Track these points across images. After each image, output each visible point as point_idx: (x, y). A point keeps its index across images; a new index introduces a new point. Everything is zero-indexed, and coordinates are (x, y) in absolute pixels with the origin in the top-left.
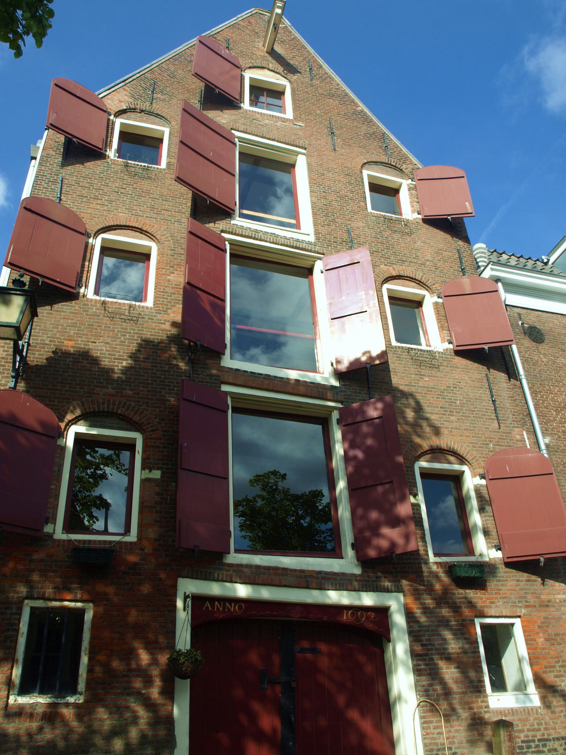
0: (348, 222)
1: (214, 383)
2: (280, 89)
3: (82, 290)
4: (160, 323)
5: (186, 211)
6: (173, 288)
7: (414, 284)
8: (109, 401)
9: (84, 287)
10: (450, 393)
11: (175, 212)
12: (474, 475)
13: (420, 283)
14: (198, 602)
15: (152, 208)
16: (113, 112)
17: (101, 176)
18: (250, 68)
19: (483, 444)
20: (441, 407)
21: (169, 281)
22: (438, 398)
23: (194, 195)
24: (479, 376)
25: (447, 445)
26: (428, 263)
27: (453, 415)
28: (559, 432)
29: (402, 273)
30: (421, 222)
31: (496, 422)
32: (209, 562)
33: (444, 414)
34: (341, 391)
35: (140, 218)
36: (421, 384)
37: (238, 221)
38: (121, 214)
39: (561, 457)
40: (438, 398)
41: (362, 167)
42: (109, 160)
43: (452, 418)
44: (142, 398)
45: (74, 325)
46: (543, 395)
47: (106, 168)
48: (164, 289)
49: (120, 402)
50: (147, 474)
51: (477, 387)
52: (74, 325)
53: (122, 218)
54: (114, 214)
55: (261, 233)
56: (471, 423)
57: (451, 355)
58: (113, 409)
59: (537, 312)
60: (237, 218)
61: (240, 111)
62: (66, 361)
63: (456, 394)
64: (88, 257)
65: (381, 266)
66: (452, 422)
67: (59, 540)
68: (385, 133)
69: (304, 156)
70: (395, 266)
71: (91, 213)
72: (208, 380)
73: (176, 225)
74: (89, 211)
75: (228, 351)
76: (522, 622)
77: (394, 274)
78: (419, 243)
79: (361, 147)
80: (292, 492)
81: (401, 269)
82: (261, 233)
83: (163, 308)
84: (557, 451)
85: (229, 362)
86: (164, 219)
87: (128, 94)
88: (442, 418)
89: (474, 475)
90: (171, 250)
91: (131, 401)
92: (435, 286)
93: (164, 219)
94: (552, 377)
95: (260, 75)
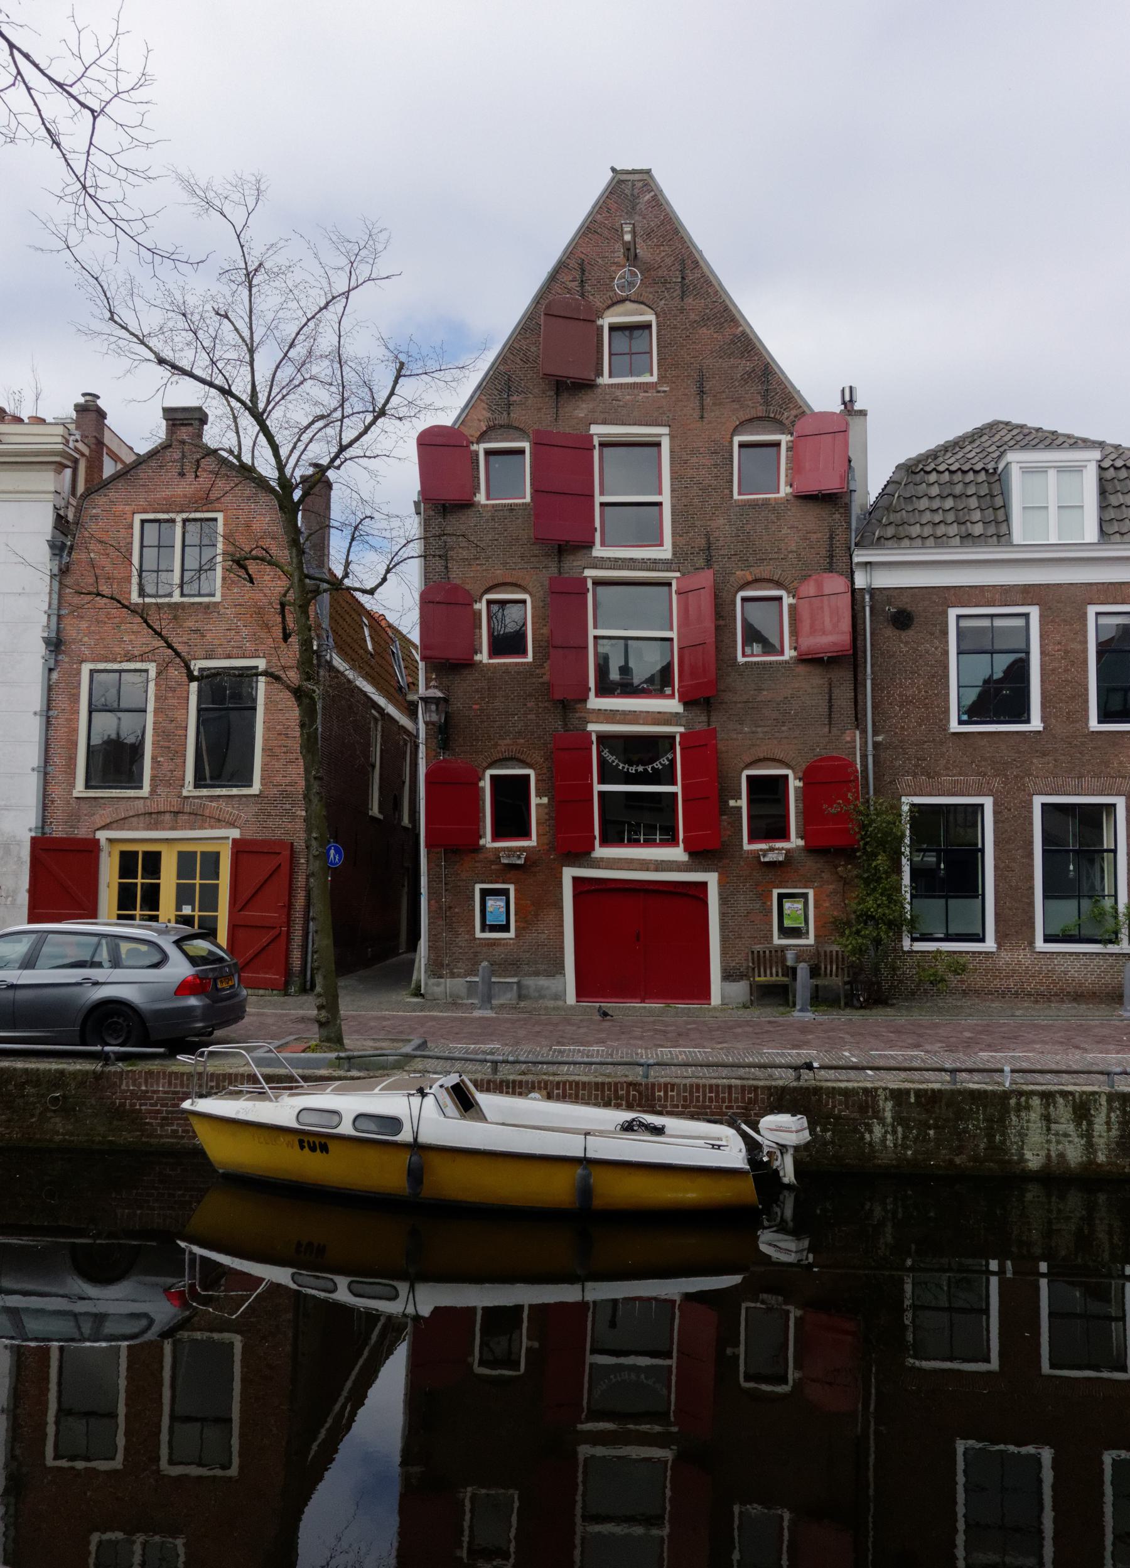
13: (779, 584)
14: (576, 880)
18: (608, 307)
23: (216, 938)
24: (821, 682)
29: (758, 576)
32: (580, 854)
36: (759, 699)
41: (734, 430)
45: (477, 691)
50: (539, 801)
52: (477, 691)
53: (500, 574)
62: (659, 1091)
70: (752, 569)
77: (750, 579)
80: (99, 402)
85: (595, 703)
89: (795, 778)
95: (620, 315)
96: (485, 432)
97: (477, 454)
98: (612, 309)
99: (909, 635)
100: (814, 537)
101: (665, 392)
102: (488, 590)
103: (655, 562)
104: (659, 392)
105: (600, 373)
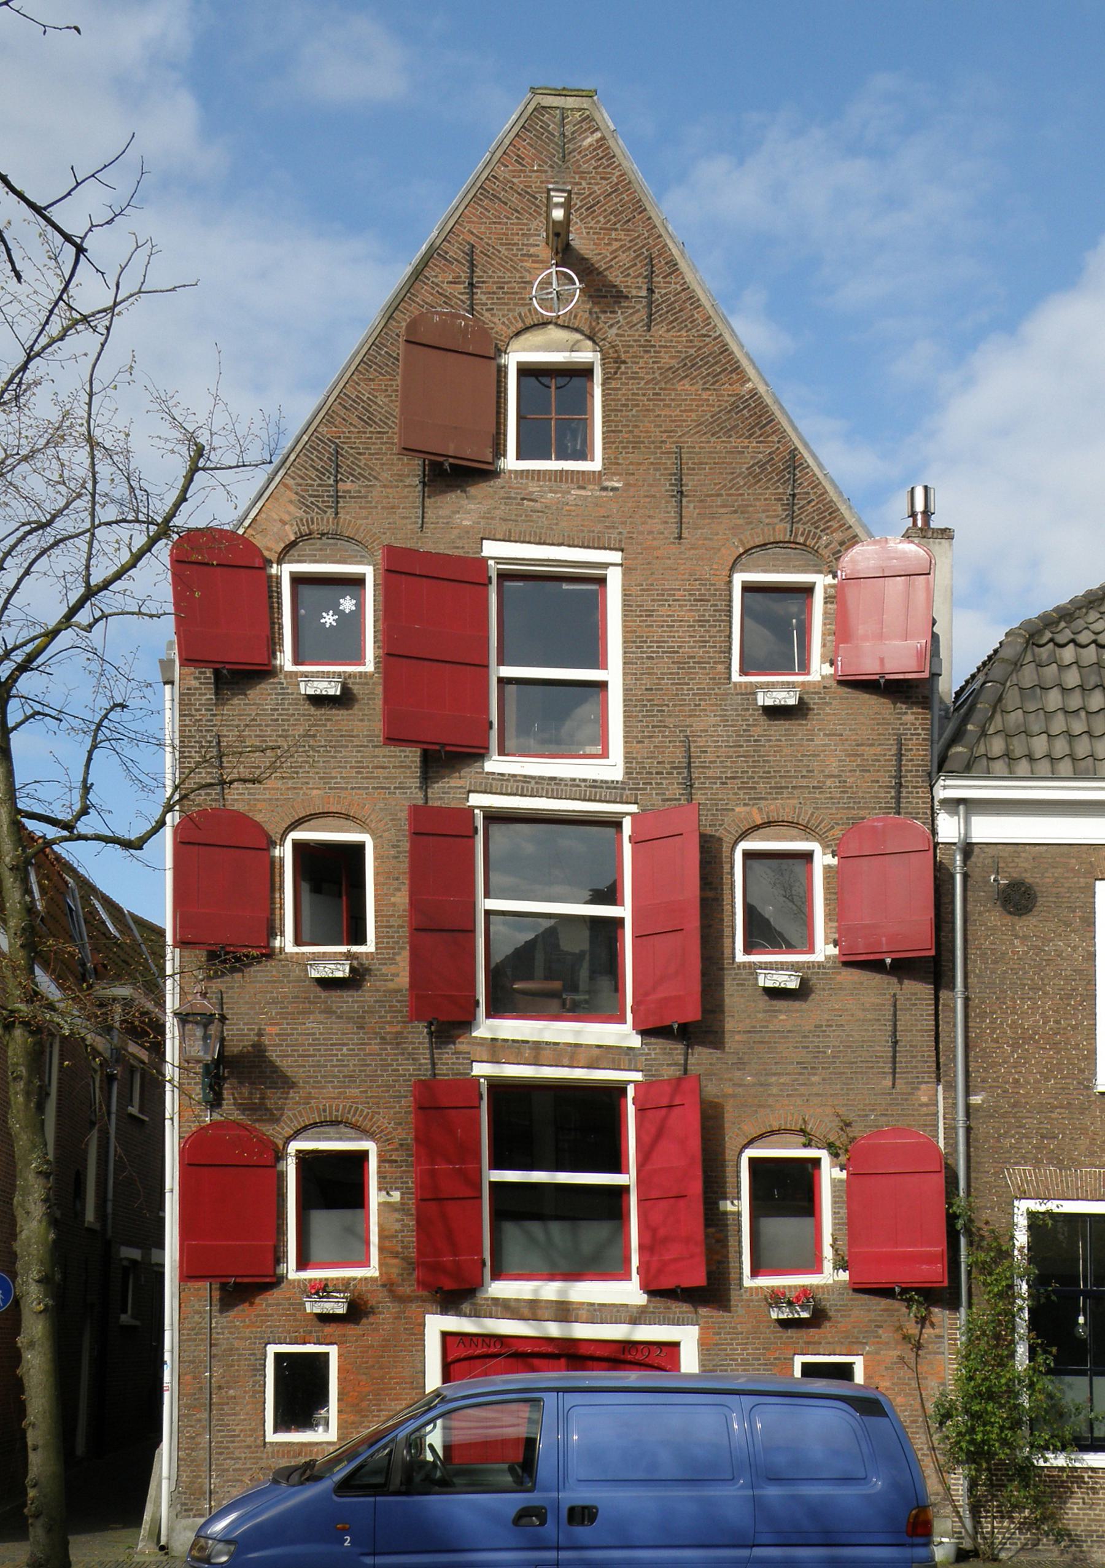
0: (688, 721)
1: (463, 1064)
2: (587, 367)
3: (277, 943)
4: (386, 981)
5: (412, 762)
6: (399, 917)
7: (795, 832)
8: (331, 1106)
9: (278, 938)
10: (818, 1036)
11: (394, 767)
12: (833, 1166)
15: (359, 768)
16: (273, 556)
17: (275, 717)
18: (518, 334)
19: (859, 1116)
20: (798, 1063)
21: (394, 905)
22: (796, 1047)
25: (409, 1113)
26: (829, 783)
27: (815, 1074)
28: (1006, 1083)
29: (774, 816)
30: (834, 684)
31: (890, 1077)
33: (800, 1074)
34: (642, 1054)
35: (343, 794)
37: (495, 764)
38: (315, 792)
39: (997, 1125)
40: (796, 1047)
42: (282, 676)
43: (814, 1079)
44: (371, 1097)
46: (997, 1018)
47: (280, 697)
48: (388, 921)
49: (344, 1107)
51: (870, 1020)
54: (305, 794)
55: (533, 782)
56: (844, 1084)
57: (834, 968)
58: (325, 1116)
59: (1041, 847)
60: (496, 757)
61: (499, 482)
63: (829, 1036)
64: (277, 885)
65: (737, 809)
66: (812, 1084)
67: (294, 1280)
68: (796, 449)
69: (620, 568)
71: (270, 799)
72: (455, 1060)
73: (398, 795)
74: (267, 796)
75: (482, 1010)
76: (865, 1361)
78: (820, 740)
79: (735, 512)
81: (772, 807)
82: (533, 782)
83: (388, 954)
84: (992, 1116)
86: (378, 788)
87: (295, 497)
88: (797, 1080)
89: (833, 1166)
90: (393, 846)
91: (357, 1103)
92: (831, 832)
93: (378, 788)
94: (1025, 982)
95: (538, 349)
96: (293, 545)
97: (279, 578)
98: (523, 338)
99: (1027, 924)
100: (869, 751)
101: (614, 489)
102: (294, 826)
103: (595, 784)
104: (605, 489)
105: (499, 451)
